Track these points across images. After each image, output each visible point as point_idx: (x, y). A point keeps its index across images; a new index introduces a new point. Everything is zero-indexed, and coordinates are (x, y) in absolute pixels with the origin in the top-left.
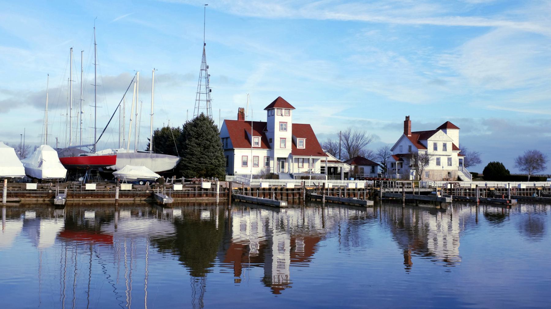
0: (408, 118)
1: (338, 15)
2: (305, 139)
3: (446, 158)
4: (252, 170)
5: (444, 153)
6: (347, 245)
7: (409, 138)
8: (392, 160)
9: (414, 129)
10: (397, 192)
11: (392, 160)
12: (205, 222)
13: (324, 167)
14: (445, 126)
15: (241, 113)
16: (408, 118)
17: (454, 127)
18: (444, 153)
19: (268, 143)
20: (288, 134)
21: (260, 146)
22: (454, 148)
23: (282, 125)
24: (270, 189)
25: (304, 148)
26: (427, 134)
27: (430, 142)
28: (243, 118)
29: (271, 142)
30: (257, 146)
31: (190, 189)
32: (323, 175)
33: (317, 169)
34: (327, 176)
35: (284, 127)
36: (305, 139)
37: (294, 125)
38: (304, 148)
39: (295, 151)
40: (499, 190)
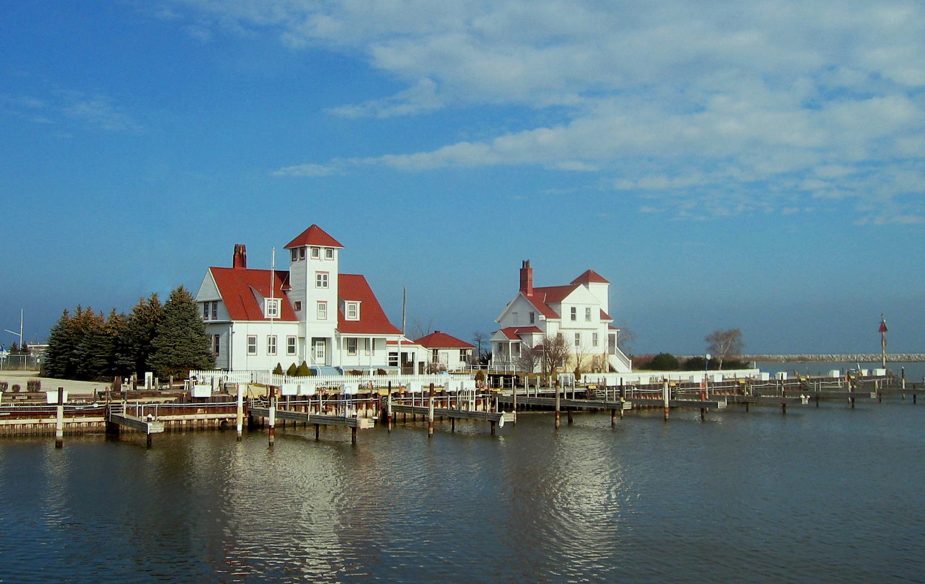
0: (526, 264)
1: (447, 151)
2: (358, 303)
3: (591, 332)
4: (264, 362)
5: (587, 325)
6: (707, 340)
7: (530, 298)
8: (501, 337)
9: (537, 280)
10: (533, 395)
11: (501, 337)
12: (766, 371)
13: (396, 354)
14: (587, 278)
15: (240, 257)
16: (526, 264)
17: (599, 279)
18: (587, 325)
19: (291, 312)
20: (331, 293)
21: (279, 317)
22: (603, 316)
23: (319, 277)
24: (315, 397)
25: (358, 319)
26: (559, 293)
27: (566, 305)
28: (243, 264)
29: (299, 308)
30: (272, 316)
31: (173, 399)
32: (393, 368)
33: (380, 358)
34: (399, 370)
35: (322, 281)
36: (358, 303)
37: (341, 277)
38: (358, 319)
39: (343, 325)
40: (683, 385)
